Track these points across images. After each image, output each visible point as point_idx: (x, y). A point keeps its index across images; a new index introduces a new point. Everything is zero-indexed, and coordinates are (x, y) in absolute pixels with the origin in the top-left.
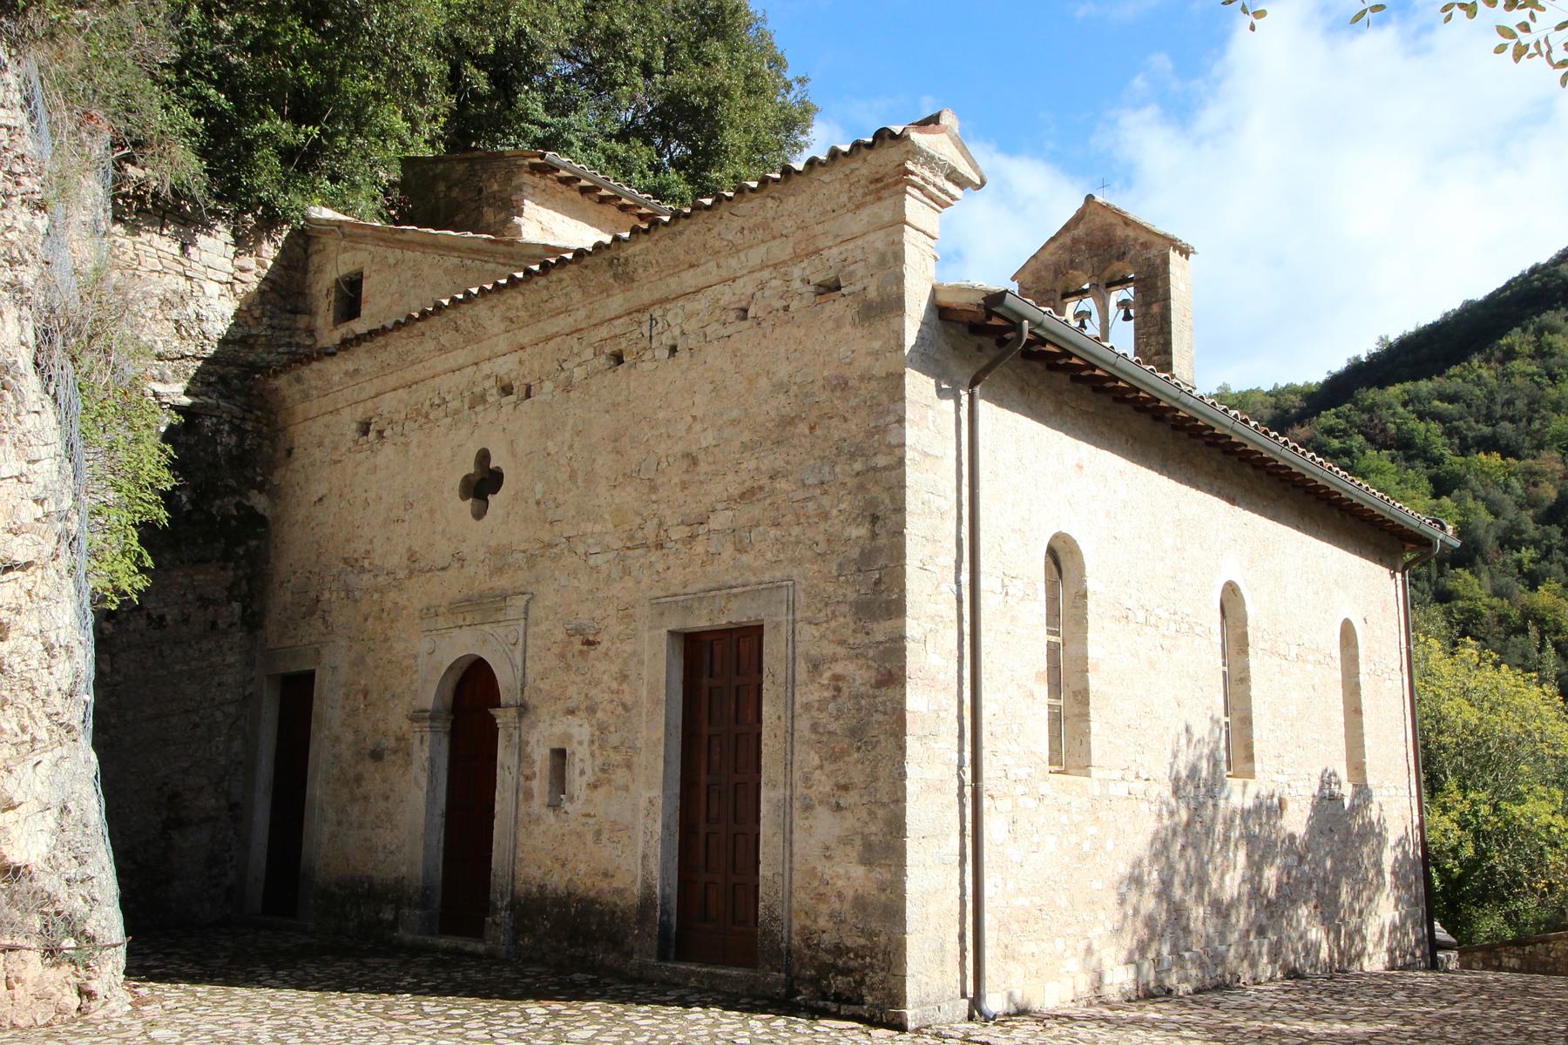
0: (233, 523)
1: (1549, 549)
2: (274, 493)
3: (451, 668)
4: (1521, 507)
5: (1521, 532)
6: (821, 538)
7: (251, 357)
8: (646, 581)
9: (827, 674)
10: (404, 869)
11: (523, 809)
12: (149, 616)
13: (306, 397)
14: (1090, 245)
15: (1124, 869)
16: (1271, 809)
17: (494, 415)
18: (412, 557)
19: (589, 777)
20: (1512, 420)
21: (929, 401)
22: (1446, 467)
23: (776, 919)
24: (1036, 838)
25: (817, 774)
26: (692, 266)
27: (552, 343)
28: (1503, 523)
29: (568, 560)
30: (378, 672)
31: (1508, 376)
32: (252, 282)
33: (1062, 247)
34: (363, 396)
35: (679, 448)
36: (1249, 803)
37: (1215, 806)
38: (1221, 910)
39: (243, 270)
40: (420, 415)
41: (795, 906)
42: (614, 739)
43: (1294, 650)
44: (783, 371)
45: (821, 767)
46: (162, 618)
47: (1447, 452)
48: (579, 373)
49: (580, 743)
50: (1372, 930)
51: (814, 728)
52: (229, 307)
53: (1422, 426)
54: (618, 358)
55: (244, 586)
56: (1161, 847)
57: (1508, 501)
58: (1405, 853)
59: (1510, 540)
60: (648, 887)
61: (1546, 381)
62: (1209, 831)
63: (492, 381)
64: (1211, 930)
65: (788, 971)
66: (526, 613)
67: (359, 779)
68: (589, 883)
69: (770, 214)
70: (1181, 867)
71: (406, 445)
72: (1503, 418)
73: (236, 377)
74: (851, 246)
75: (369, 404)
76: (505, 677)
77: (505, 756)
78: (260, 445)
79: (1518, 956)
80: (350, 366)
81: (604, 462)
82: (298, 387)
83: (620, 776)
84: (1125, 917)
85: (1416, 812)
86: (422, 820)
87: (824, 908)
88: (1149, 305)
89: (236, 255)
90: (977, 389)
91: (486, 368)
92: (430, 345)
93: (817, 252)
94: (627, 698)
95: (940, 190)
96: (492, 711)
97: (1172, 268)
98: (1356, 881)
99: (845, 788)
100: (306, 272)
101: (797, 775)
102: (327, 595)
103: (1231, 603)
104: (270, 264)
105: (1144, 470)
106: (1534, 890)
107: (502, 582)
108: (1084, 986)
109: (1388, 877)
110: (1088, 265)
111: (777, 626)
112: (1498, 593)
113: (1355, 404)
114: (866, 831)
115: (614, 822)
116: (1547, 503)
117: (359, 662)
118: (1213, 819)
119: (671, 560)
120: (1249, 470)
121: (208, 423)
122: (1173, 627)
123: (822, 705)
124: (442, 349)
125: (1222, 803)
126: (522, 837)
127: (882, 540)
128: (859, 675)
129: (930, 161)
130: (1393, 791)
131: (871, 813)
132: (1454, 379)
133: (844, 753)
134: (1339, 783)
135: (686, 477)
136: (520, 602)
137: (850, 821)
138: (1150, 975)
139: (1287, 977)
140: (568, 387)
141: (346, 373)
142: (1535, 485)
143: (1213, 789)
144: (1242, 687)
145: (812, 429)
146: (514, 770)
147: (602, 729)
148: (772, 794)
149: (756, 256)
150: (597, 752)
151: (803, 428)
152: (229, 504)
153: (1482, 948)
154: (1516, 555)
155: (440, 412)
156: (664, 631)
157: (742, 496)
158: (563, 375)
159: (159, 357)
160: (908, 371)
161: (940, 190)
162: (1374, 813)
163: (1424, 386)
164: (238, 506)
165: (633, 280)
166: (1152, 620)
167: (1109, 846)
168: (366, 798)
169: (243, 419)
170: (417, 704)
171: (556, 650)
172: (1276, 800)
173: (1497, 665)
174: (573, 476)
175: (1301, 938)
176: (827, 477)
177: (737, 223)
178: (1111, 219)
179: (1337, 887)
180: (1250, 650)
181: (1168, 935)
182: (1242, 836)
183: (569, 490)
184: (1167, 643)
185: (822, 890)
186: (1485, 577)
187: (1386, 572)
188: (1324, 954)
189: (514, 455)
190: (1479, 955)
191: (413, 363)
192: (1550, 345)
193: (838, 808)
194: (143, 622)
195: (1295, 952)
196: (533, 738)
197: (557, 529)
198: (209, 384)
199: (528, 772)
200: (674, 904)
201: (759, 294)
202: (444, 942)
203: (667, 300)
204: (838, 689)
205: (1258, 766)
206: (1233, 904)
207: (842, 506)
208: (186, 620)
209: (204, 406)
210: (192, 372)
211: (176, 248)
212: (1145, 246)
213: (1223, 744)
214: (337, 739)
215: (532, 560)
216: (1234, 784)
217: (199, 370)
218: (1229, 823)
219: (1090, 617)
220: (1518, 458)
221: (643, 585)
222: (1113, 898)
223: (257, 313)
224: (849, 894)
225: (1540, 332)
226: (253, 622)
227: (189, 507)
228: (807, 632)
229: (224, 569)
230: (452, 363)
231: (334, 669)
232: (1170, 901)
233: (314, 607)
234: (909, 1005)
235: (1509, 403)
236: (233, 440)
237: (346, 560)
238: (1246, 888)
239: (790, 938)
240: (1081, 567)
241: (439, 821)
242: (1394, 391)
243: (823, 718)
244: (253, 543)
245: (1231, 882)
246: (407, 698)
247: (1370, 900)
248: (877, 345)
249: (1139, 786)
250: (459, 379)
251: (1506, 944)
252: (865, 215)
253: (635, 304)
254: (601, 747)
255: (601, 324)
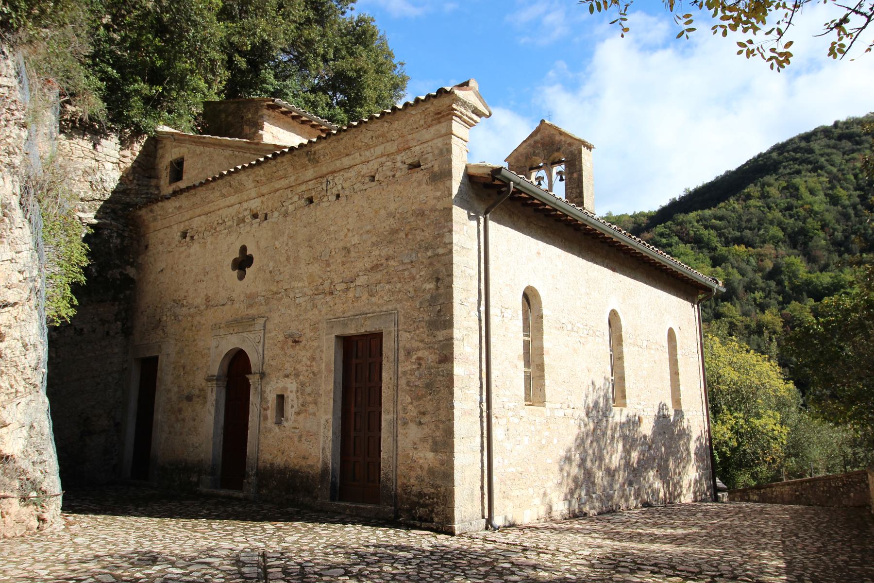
0: (118, 282)
1: (770, 292)
2: (139, 268)
3: (227, 354)
4: (755, 271)
5: (756, 284)
6: (411, 289)
7: (128, 200)
8: (324, 311)
9: (415, 357)
10: (203, 455)
11: (262, 425)
12: (75, 329)
13: (155, 219)
14: (543, 144)
15: (562, 453)
16: (634, 423)
17: (249, 228)
18: (208, 299)
19: (296, 409)
20: (750, 229)
21: (464, 222)
22: (718, 252)
23: (389, 480)
24: (518, 438)
25: (410, 407)
26: (347, 155)
27: (278, 193)
28: (746, 279)
29: (286, 300)
30: (190, 357)
31: (748, 207)
32: (129, 163)
33: (530, 145)
34: (184, 219)
35: (341, 245)
36: (624, 420)
37: (607, 421)
38: (611, 473)
39: (124, 157)
40: (212, 229)
41: (399, 473)
42: (308, 390)
43: (645, 343)
44: (392, 207)
45: (412, 403)
46: (82, 330)
47: (719, 245)
48: (291, 208)
49: (291, 392)
50: (685, 483)
51: (408, 383)
52: (117, 175)
53: (706, 232)
54: (310, 201)
55: (123, 314)
56: (581, 442)
57: (749, 268)
58: (701, 444)
59: (750, 288)
60: (325, 464)
61: (766, 210)
62: (604, 434)
63: (248, 212)
64: (606, 483)
65: (396, 505)
66: (265, 327)
67: (180, 410)
68: (296, 462)
69: (386, 130)
70: (590, 452)
71: (205, 243)
72: (746, 228)
73: (121, 209)
74: (425, 145)
75: (187, 223)
76: (253, 358)
77: (254, 398)
78: (132, 243)
79: (758, 495)
80: (177, 204)
81: (304, 252)
82: (151, 215)
83: (311, 408)
84: (563, 477)
85: (706, 423)
86: (212, 431)
87: (413, 474)
88: (572, 173)
89: (121, 149)
90: (488, 216)
91: (245, 205)
92: (217, 194)
93: (409, 148)
94: (315, 369)
95: (469, 118)
96: (247, 376)
97: (583, 155)
98: (677, 458)
99: (424, 414)
100: (155, 157)
101: (400, 407)
102: (165, 318)
103: (614, 320)
104: (137, 153)
105: (570, 255)
106: (765, 462)
107: (252, 312)
108: (542, 511)
109: (693, 456)
110: (542, 154)
111: (390, 333)
112: (745, 314)
113: (674, 221)
114: (434, 435)
115: (308, 432)
116: (768, 270)
117: (181, 352)
118: (606, 427)
119: (337, 300)
120: (622, 255)
121: (106, 232)
122: (585, 332)
123: (412, 372)
124: (223, 196)
125: (610, 420)
126: (262, 440)
127: (441, 291)
128: (430, 358)
129: (464, 104)
130: (695, 413)
131: (436, 426)
132: (721, 209)
133: (424, 396)
134: (667, 409)
135: (344, 259)
136: (261, 321)
137: (426, 430)
138: (575, 505)
139: (643, 506)
140: (286, 214)
141: (175, 208)
142: (762, 261)
143: (606, 413)
144: (620, 362)
145: (407, 235)
146: (258, 406)
147: (303, 385)
148: (387, 417)
149: (379, 150)
150: (300, 396)
151: (402, 235)
152: (116, 273)
153: (740, 491)
154: (752, 295)
155: (222, 227)
156: (333, 335)
157: (372, 268)
158: (283, 209)
159: (82, 200)
160: (454, 206)
161: (469, 118)
162: (685, 424)
163: (707, 212)
164: (121, 274)
165: (318, 162)
166: (575, 329)
167: (555, 441)
168: (184, 420)
169: (124, 231)
170: (210, 373)
171: (279, 345)
172: (637, 418)
173: (748, 351)
174: (288, 259)
175: (650, 487)
176: (414, 259)
177: (369, 134)
178: (553, 132)
179: (667, 460)
180: (624, 344)
181: (584, 486)
182: (620, 436)
183: (286, 266)
184: (582, 340)
185: (412, 465)
186: (738, 306)
187: (690, 304)
188: (661, 495)
189: (259, 248)
190: (738, 494)
191: (209, 203)
192: (768, 192)
193: (420, 423)
194: (72, 332)
195: (648, 494)
196: (268, 389)
197: (280, 284)
198: (107, 213)
199: (265, 406)
200: (338, 472)
201: (380, 169)
202: (223, 492)
203: (335, 172)
204: (420, 364)
205: (628, 401)
206: (617, 470)
207: (422, 274)
208: (94, 331)
209: (105, 224)
210: (98, 207)
211: (90, 146)
212: (570, 145)
213: (610, 390)
214: (169, 390)
215: (267, 300)
216: (616, 410)
217: (102, 206)
218: (614, 430)
219: (544, 328)
220: (754, 248)
221: (323, 313)
222: (556, 468)
223: (131, 178)
224: (426, 467)
225: (763, 185)
226: (127, 332)
227: (96, 274)
228: (404, 336)
229: (113, 305)
230: (228, 203)
231: (168, 355)
232: (585, 469)
233: (158, 324)
234: (456, 522)
235: (749, 220)
236: (119, 241)
237: (174, 301)
238: (622, 462)
239: (396, 489)
240: (540, 303)
241: (221, 431)
242: (693, 215)
243: (413, 378)
244: (128, 292)
245: (615, 459)
246: (205, 370)
247: (684, 467)
248: (438, 194)
249: (569, 411)
250: (232, 211)
251: (752, 488)
252: (432, 130)
253: (320, 174)
254: (302, 394)
255: (302, 183)
